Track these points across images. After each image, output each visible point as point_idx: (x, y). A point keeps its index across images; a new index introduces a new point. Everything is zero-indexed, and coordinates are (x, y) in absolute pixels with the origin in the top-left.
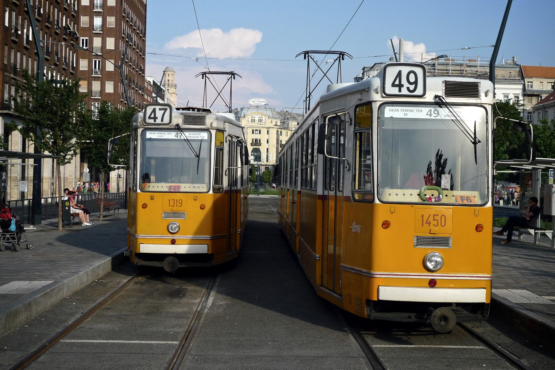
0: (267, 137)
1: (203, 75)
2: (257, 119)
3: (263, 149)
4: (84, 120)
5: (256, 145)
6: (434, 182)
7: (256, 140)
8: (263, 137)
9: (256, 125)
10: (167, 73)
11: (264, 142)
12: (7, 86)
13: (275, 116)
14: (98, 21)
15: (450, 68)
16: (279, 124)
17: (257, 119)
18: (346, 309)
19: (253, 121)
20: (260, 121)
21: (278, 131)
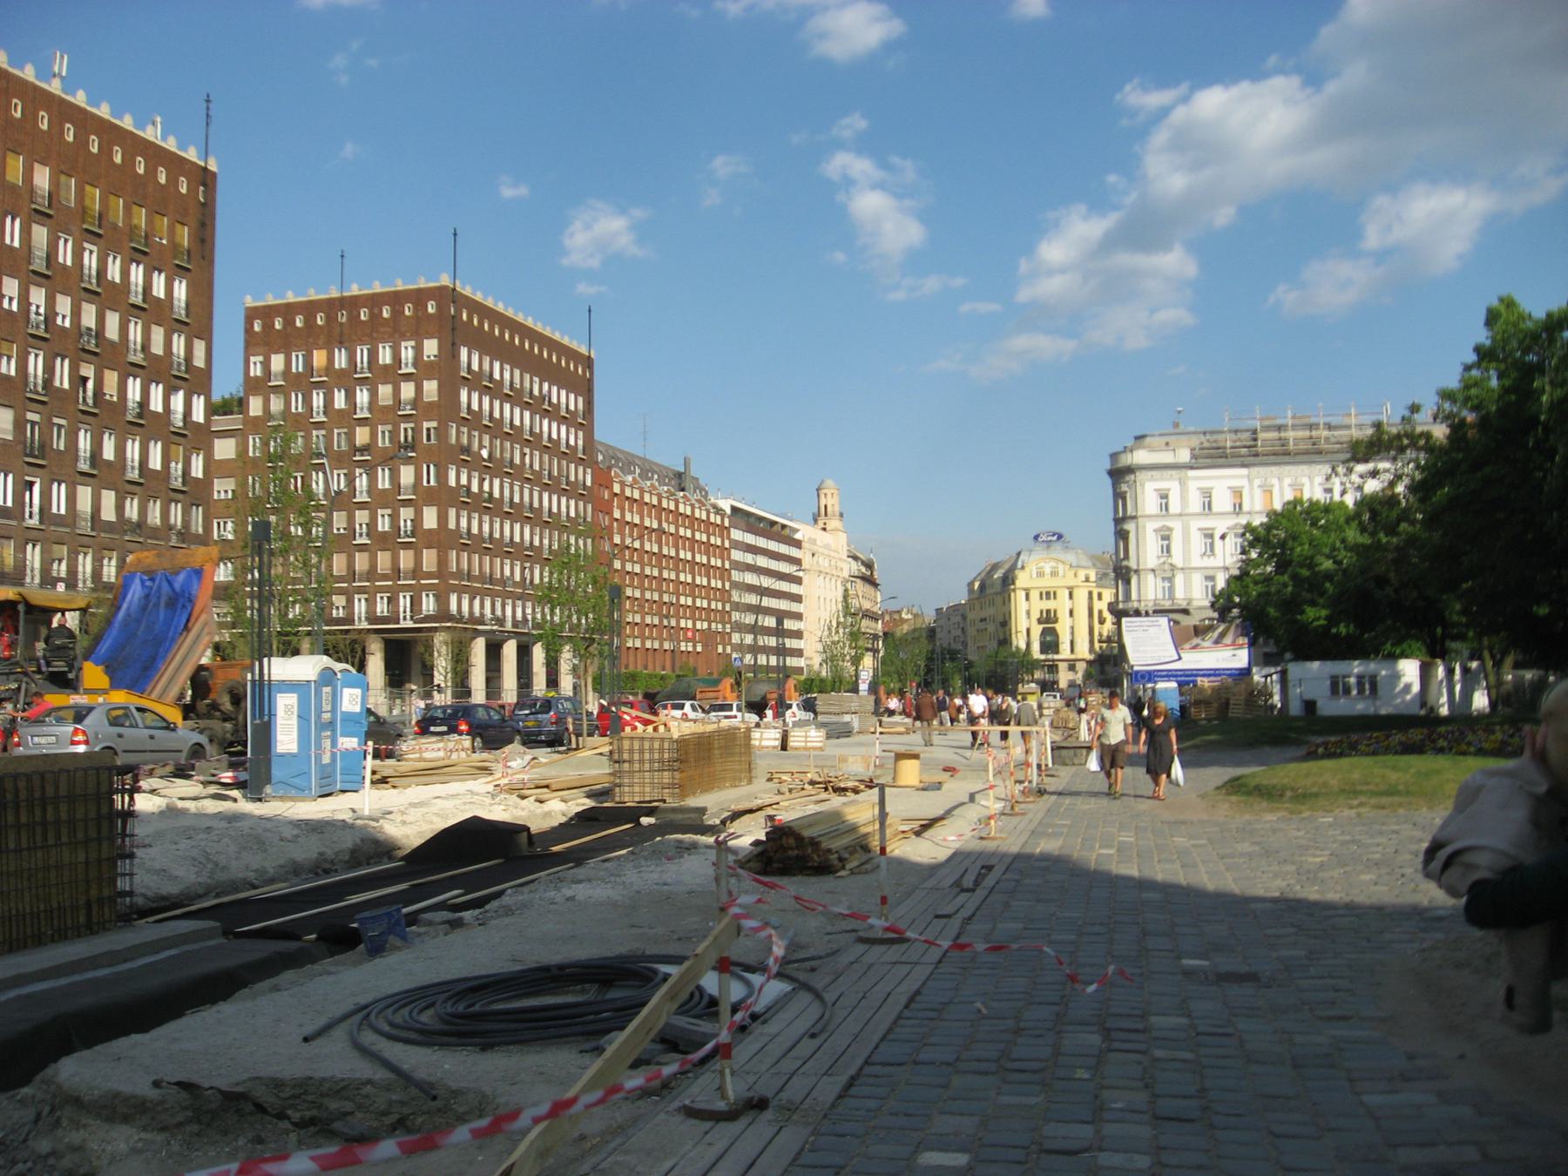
0: (1068, 604)
1: (679, 475)
2: (1048, 570)
3: (1063, 628)
4: (1461, 637)
5: (1048, 620)
6: (1354, 692)
7: (1048, 611)
8: (1061, 605)
9: (1047, 583)
10: (822, 493)
11: (1063, 616)
12: (55, 485)
13: (1084, 563)
14: (362, 397)
15: (1291, 434)
16: (1093, 577)
17: (1048, 570)
18: (417, 842)
19: (1040, 574)
20: (1054, 574)
21: (1090, 593)
